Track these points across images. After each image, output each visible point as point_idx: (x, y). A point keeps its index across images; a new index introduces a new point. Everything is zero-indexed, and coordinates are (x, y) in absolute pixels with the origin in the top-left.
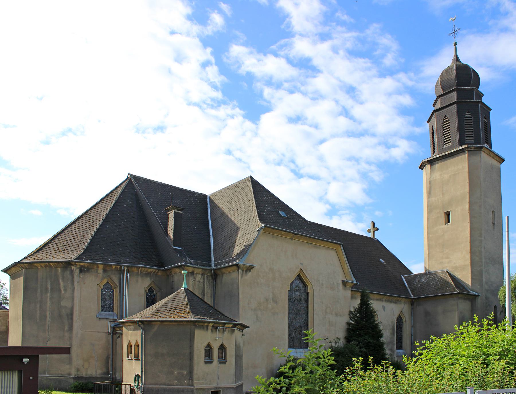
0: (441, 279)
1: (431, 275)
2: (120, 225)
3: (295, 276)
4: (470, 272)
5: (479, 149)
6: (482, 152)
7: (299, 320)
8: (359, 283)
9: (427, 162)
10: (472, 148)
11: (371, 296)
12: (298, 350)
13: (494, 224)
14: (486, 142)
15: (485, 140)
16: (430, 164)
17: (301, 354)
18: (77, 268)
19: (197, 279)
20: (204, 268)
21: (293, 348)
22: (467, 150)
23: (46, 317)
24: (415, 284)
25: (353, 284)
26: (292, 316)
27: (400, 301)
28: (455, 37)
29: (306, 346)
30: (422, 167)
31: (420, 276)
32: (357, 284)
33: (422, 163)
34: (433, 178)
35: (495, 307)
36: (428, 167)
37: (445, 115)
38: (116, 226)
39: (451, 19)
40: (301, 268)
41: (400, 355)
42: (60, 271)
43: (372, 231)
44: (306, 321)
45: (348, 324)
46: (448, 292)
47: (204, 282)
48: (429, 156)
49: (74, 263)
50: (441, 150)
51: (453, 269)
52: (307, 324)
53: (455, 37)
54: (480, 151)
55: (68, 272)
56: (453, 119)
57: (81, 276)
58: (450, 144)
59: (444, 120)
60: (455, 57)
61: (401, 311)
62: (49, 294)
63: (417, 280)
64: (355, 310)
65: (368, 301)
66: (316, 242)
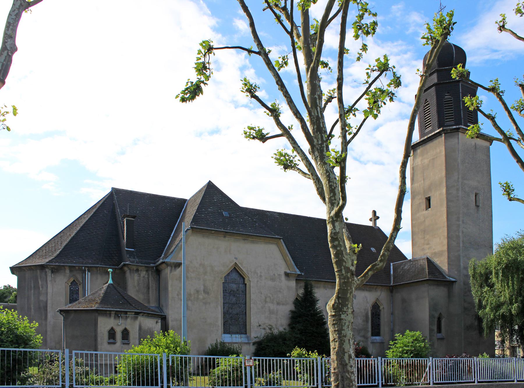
2: (92, 233)
8: (303, 274)
10: (448, 130)
12: (234, 336)
17: (237, 339)
18: (50, 270)
19: (142, 275)
20: (146, 265)
21: (229, 334)
23: (31, 309)
26: (228, 305)
27: (376, 289)
29: (245, 332)
32: (301, 274)
34: (416, 164)
38: (89, 234)
41: (376, 342)
43: (373, 220)
47: (148, 278)
49: (46, 266)
51: (433, 255)
54: (458, 132)
55: (44, 273)
56: (432, 102)
57: (53, 276)
58: (430, 128)
59: (425, 104)
62: (32, 291)
66: (253, 238)
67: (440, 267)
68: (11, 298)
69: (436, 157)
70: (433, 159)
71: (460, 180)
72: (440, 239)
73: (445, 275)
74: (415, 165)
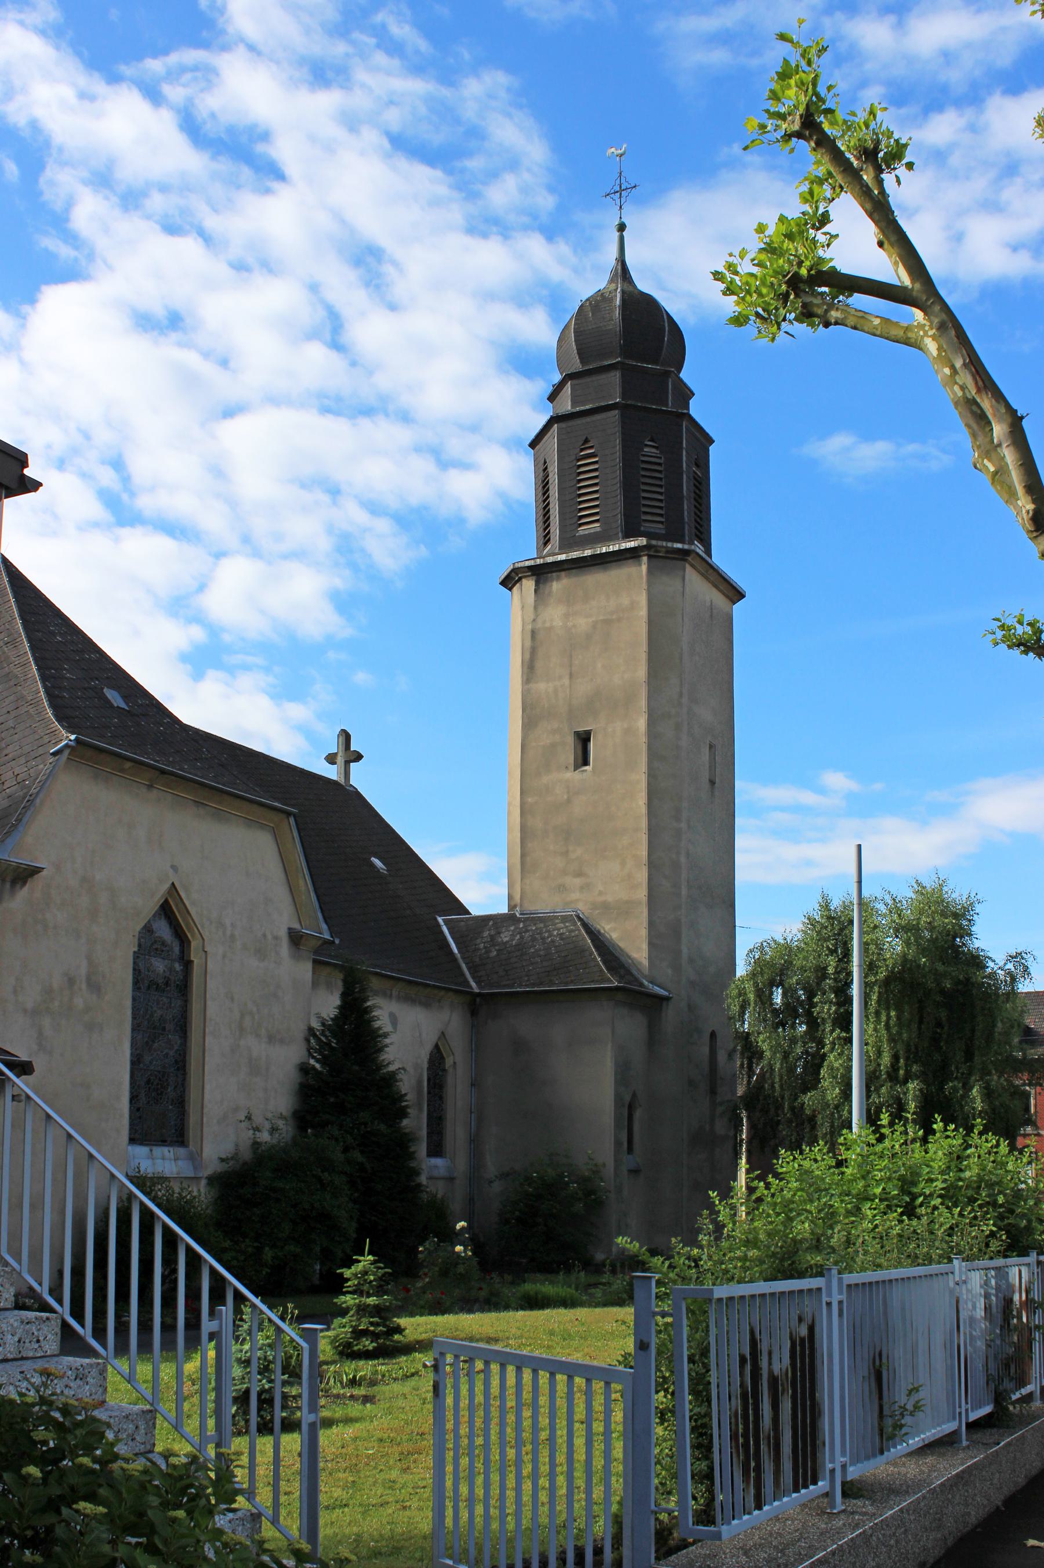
0: (562, 939)
1: (528, 923)
3: (153, 905)
4: (645, 924)
5: (680, 557)
6: (688, 566)
7: (162, 1052)
8: (337, 941)
11: (375, 983)
12: (158, 1151)
13: (712, 782)
14: (696, 535)
15: (694, 530)
16: (534, 578)
22: (644, 555)
24: (479, 949)
25: (320, 942)
27: (439, 1001)
28: (621, 207)
30: (509, 581)
31: (495, 924)
32: (333, 942)
33: (513, 571)
34: (544, 622)
35: (713, 1035)
36: (529, 584)
37: (587, 438)
39: (613, 150)
40: (173, 884)
43: (340, 760)
44: (180, 1054)
45: (304, 1069)
46: (585, 983)
48: (528, 552)
50: (567, 544)
52: (185, 1066)
53: (621, 207)
59: (582, 450)
60: (619, 267)
61: (443, 1033)
63: (486, 934)
64: (323, 1024)
65: (366, 1000)
67: (621, 950)
68: (884, 1077)
69: (619, 620)
70: (607, 622)
71: (685, 700)
72: (623, 864)
73: (639, 977)
74: (539, 625)
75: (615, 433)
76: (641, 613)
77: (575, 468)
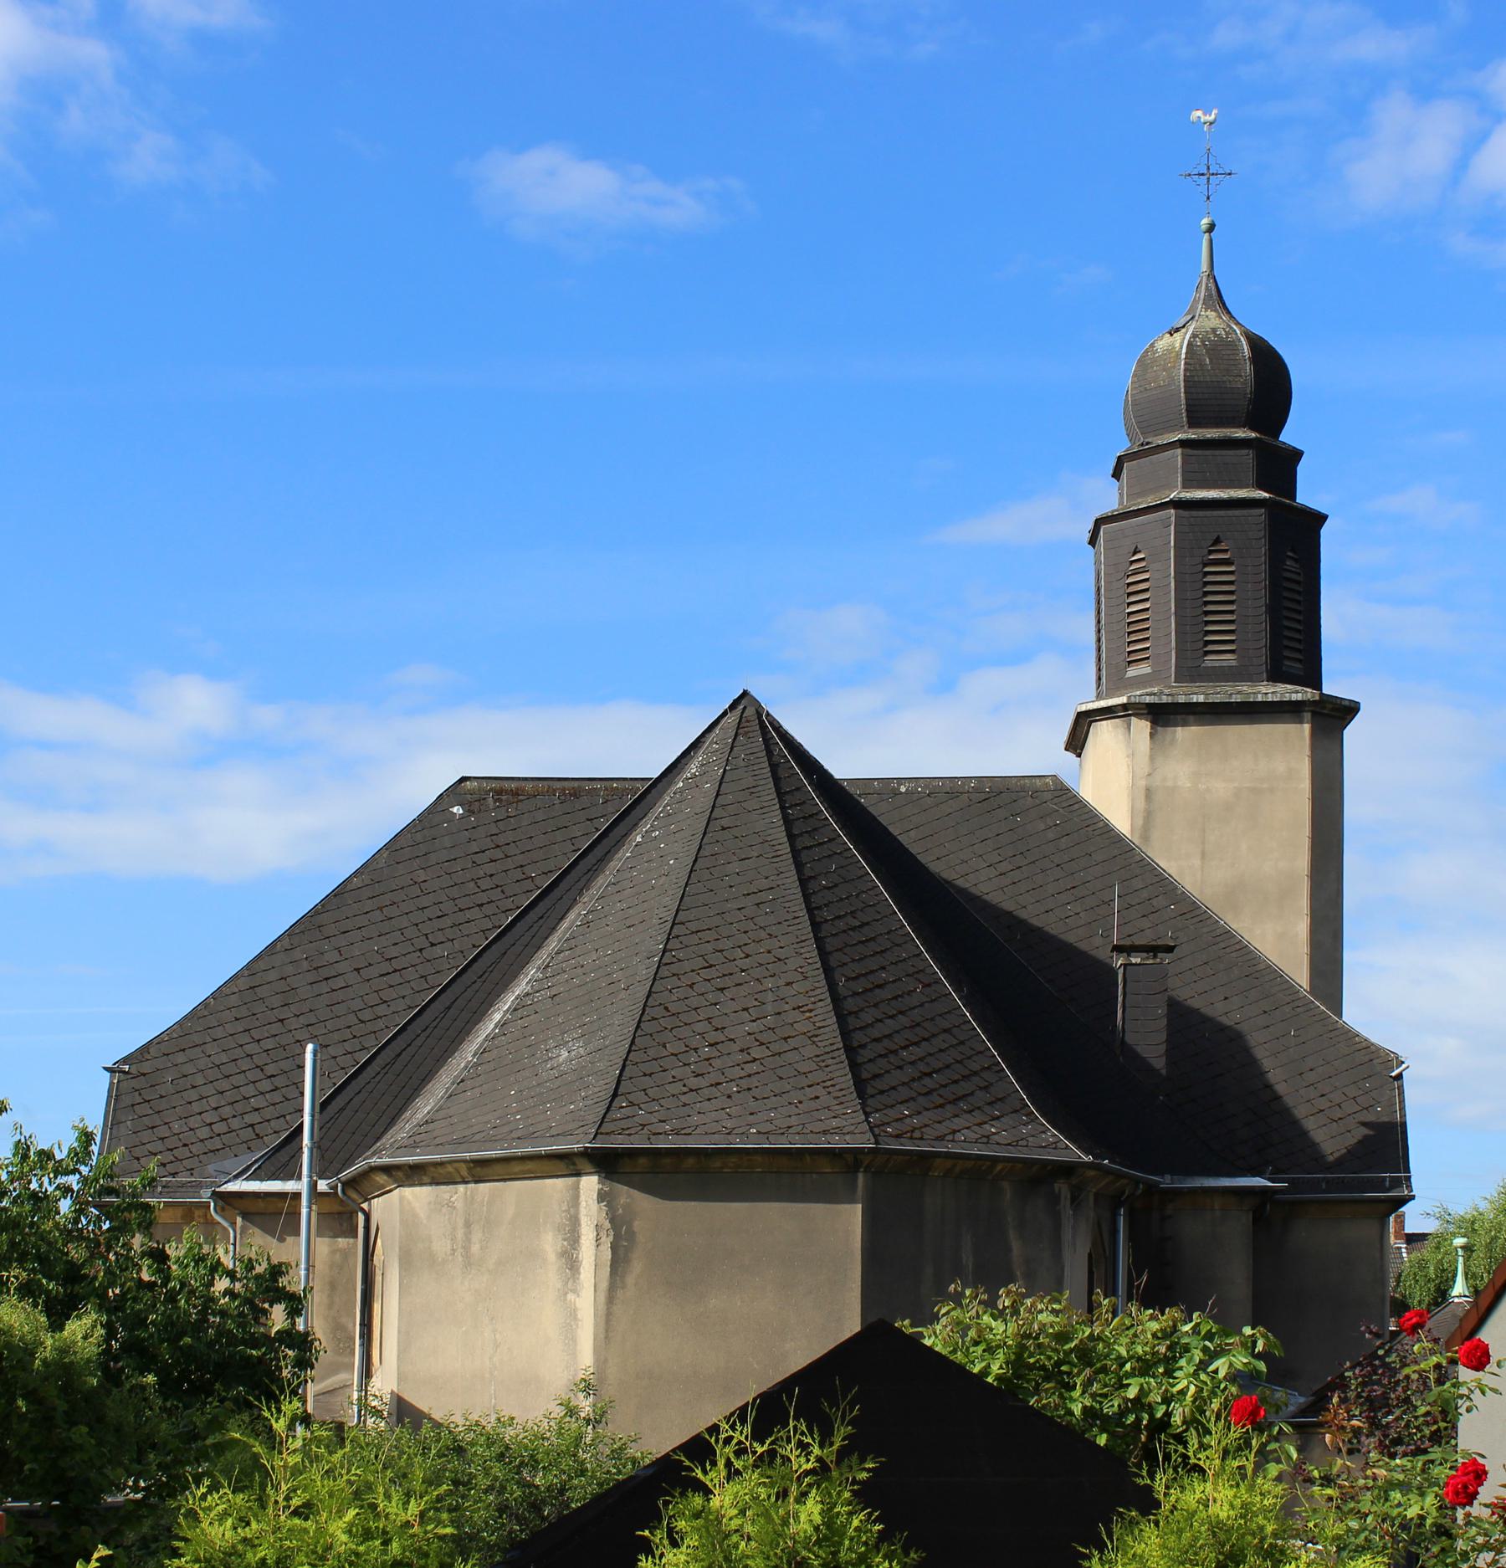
9: (1144, 706)
22: (1308, 711)
39: (1199, 113)
42: (1008, 1196)
59: (1211, 552)
75: (1260, 539)
76: (1302, 786)
77: (1201, 575)
